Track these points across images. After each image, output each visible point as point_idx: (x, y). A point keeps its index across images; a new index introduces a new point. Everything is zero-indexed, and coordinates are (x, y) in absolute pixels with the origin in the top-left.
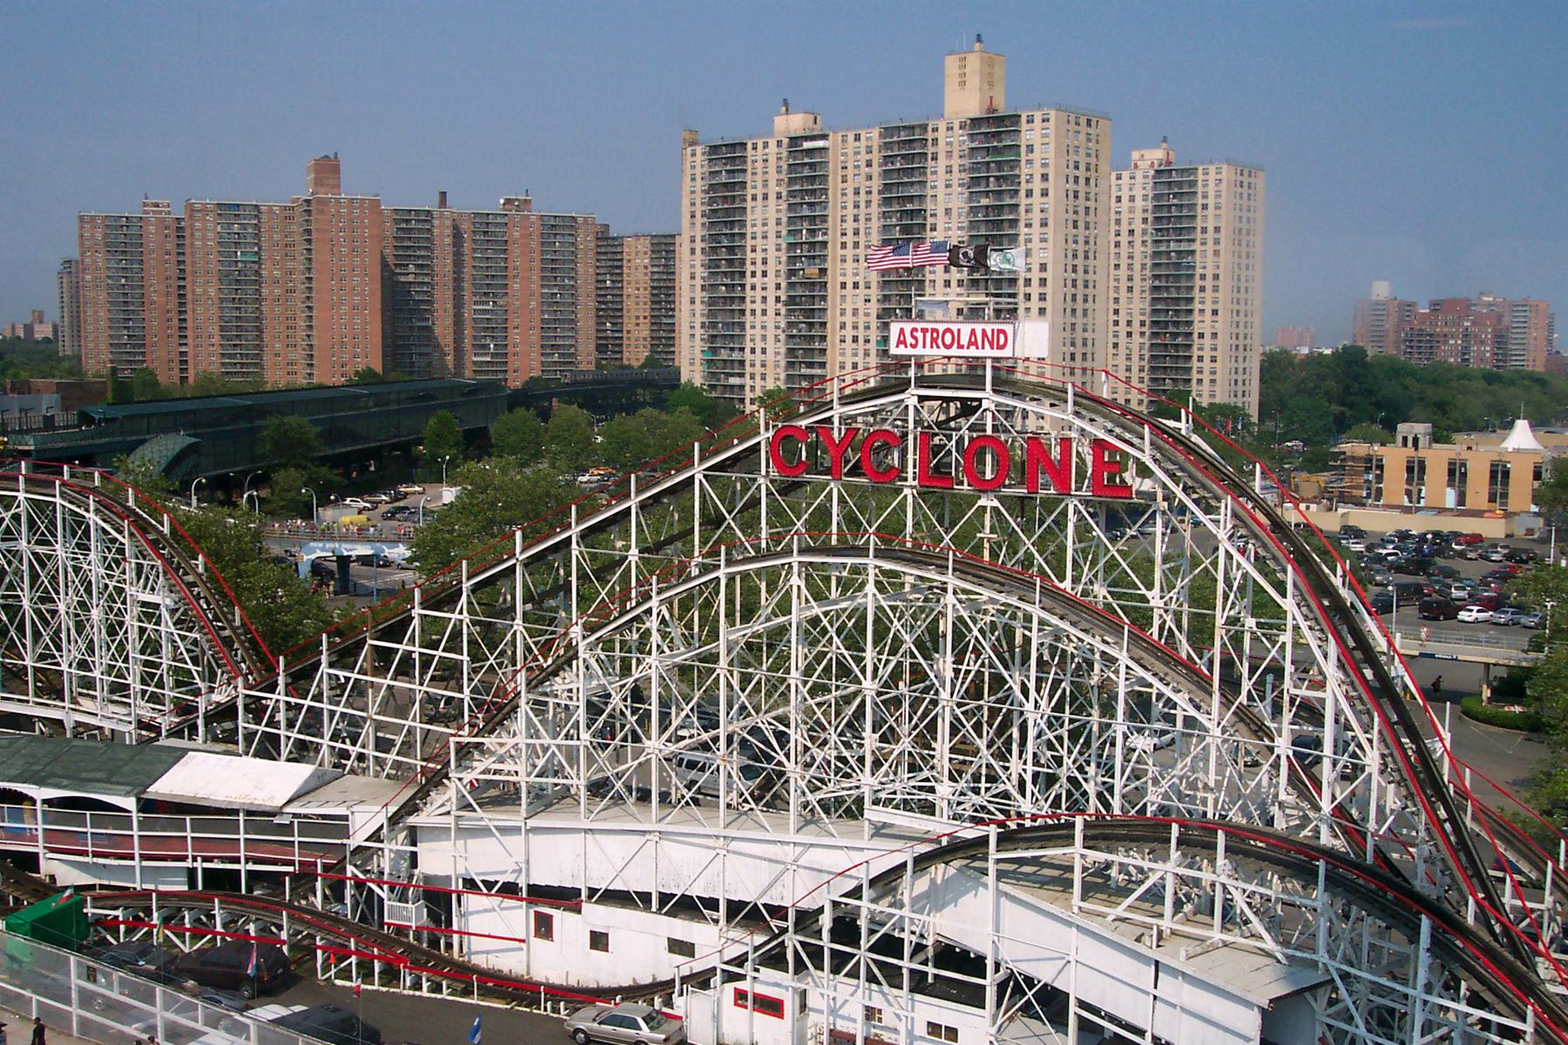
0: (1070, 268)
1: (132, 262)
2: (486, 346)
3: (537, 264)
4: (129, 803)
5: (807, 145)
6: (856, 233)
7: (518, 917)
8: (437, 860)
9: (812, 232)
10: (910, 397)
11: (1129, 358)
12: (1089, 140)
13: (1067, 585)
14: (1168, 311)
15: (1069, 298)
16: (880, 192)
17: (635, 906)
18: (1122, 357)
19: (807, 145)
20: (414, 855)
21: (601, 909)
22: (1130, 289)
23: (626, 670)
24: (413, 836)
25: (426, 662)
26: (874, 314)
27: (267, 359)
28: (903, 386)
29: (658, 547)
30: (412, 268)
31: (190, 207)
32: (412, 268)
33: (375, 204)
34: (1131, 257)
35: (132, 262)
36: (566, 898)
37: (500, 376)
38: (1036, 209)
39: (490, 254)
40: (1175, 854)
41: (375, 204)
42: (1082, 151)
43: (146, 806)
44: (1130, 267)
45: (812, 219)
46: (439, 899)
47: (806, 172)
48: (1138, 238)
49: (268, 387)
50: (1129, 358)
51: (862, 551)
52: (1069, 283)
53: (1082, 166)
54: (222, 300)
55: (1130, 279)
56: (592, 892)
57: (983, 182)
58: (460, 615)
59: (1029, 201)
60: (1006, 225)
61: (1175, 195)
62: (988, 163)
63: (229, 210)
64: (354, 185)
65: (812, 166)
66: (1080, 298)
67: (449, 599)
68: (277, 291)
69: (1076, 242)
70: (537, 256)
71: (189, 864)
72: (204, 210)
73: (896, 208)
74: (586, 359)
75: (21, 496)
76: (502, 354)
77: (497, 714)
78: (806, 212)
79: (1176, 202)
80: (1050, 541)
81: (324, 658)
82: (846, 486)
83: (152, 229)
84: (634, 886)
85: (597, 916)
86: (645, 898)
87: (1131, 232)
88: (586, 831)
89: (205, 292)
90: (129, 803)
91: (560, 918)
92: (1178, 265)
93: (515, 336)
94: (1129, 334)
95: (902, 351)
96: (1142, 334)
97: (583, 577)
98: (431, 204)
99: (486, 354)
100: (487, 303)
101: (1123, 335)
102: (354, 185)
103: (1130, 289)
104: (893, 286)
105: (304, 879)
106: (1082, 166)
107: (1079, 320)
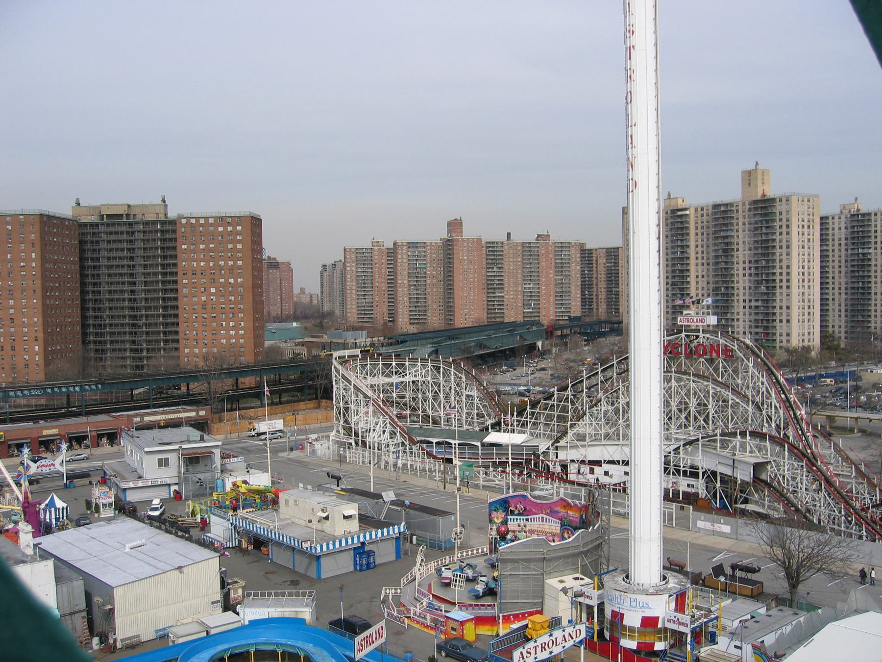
0: (801, 267)
1: (367, 268)
2: (530, 305)
3: (553, 265)
4: (479, 444)
5: (679, 213)
6: (703, 252)
7: (585, 469)
8: (562, 455)
9: (682, 253)
10: (683, 335)
11: (840, 305)
12: (809, 208)
13: (720, 379)
14: (858, 282)
15: (801, 281)
16: (713, 234)
17: (615, 464)
18: (837, 305)
19: (679, 213)
20: (557, 453)
21: (607, 465)
22: (840, 272)
23: (613, 404)
24: (557, 448)
25: (558, 406)
26: (711, 289)
27: (429, 313)
28: (681, 332)
29: (621, 374)
30: (495, 269)
31: (395, 244)
32: (495, 269)
33: (479, 240)
34: (840, 257)
35: (367, 268)
36: (598, 463)
37: (537, 318)
38: (784, 241)
39: (531, 261)
40: (739, 437)
41: (479, 240)
42: (806, 214)
43: (483, 445)
44: (840, 261)
45: (682, 247)
46: (564, 467)
47: (679, 225)
48: (843, 248)
49: (456, 327)
50: (840, 305)
51: (671, 372)
52: (801, 274)
53: (806, 220)
54: (410, 286)
55: (840, 267)
56: (605, 461)
57: (760, 229)
58: (569, 392)
59: (781, 237)
60: (770, 248)
61: (861, 226)
62: (761, 221)
63: (412, 245)
64: (469, 232)
65: (682, 223)
66: (806, 280)
67: (565, 389)
68: (434, 281)
69: (804, 255)
70: (553, 262)
71: (494, 460)
72: (402, 245)
73: (720, 241)
74: (576, 309)
75: (429, 364)
76: (537, 308)
77: (580, 417)
78: (679, 243)
79: (861, 229)
80: (716, 370)
81: (528, 407)
82: (668, 357)
83: (376, 253)
84: (615, 459)
85: (606, 467)
86: (618, 462)
87: (840, 245)
88: (603, 445)
89: (403, 282)
90: (479, 444)
91: (596, 468)
92: (863, 260)
93: (543, 301)
94: (840, 294)
95: (681, 323)
96: (846, 294)
97: (602, 382)
98: (504, 238)
99: (529, 308)
100: (530, 284)
101: (837, 294)
102: (469, 232)
103: (840, 272)
104: (720, 277)
105: (528, 461)
106: (806, 220)
107: (806, 290)
